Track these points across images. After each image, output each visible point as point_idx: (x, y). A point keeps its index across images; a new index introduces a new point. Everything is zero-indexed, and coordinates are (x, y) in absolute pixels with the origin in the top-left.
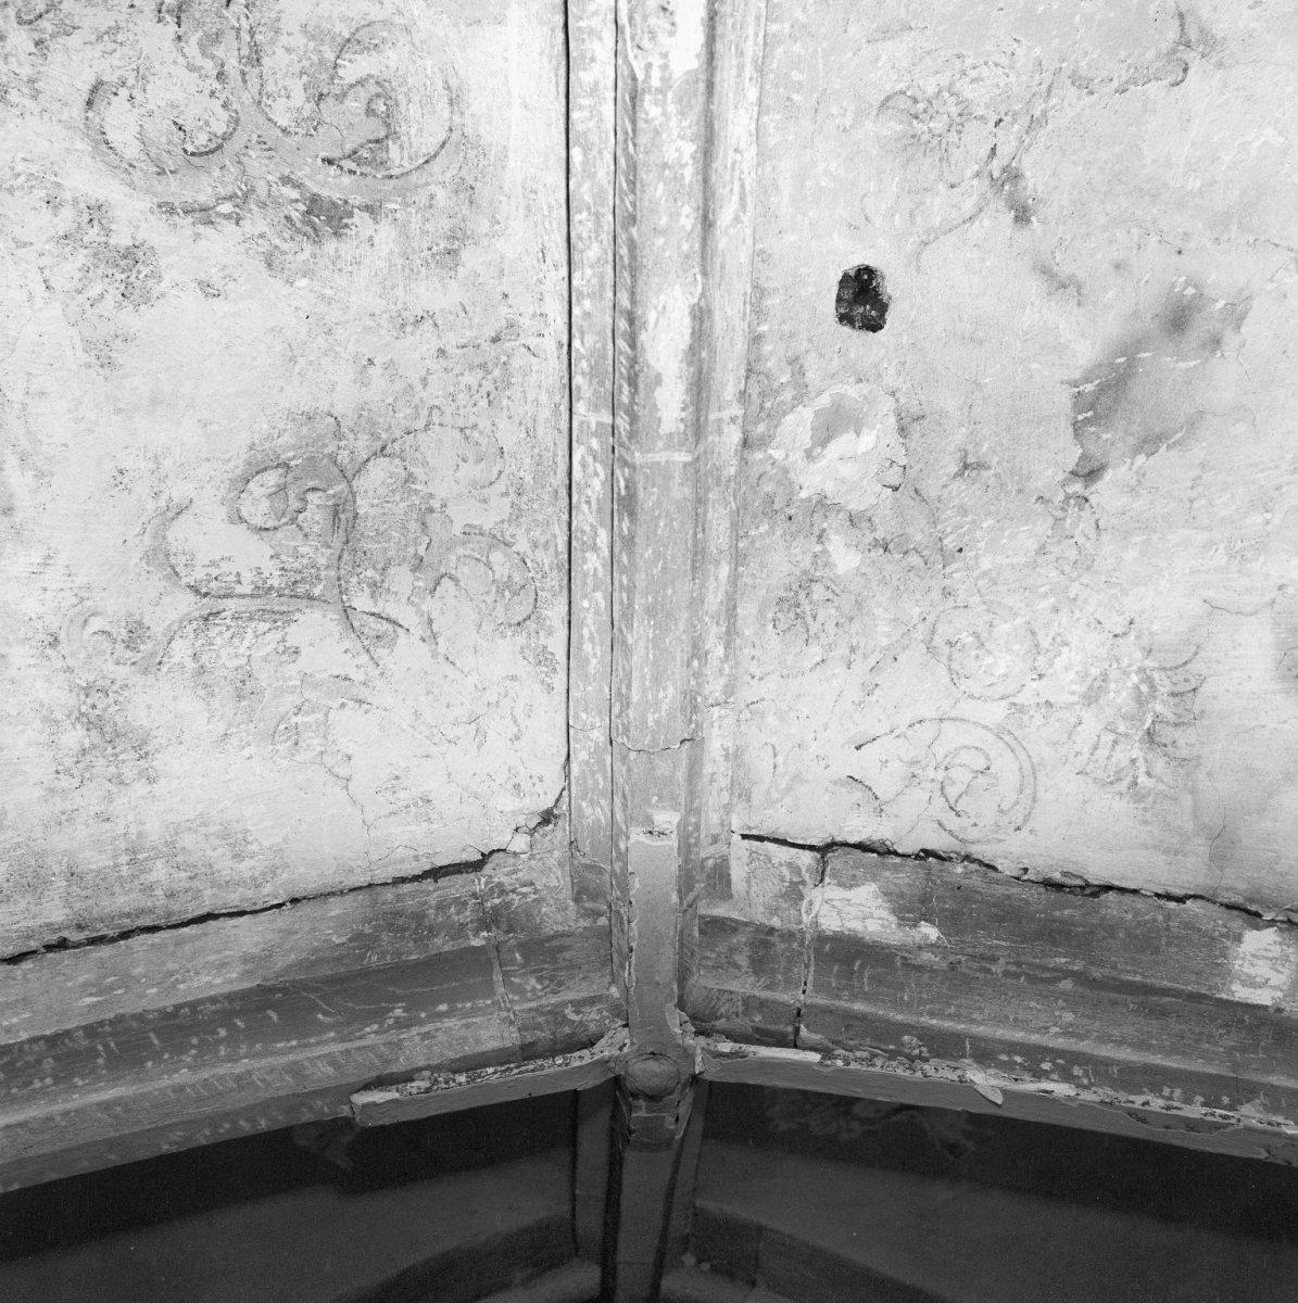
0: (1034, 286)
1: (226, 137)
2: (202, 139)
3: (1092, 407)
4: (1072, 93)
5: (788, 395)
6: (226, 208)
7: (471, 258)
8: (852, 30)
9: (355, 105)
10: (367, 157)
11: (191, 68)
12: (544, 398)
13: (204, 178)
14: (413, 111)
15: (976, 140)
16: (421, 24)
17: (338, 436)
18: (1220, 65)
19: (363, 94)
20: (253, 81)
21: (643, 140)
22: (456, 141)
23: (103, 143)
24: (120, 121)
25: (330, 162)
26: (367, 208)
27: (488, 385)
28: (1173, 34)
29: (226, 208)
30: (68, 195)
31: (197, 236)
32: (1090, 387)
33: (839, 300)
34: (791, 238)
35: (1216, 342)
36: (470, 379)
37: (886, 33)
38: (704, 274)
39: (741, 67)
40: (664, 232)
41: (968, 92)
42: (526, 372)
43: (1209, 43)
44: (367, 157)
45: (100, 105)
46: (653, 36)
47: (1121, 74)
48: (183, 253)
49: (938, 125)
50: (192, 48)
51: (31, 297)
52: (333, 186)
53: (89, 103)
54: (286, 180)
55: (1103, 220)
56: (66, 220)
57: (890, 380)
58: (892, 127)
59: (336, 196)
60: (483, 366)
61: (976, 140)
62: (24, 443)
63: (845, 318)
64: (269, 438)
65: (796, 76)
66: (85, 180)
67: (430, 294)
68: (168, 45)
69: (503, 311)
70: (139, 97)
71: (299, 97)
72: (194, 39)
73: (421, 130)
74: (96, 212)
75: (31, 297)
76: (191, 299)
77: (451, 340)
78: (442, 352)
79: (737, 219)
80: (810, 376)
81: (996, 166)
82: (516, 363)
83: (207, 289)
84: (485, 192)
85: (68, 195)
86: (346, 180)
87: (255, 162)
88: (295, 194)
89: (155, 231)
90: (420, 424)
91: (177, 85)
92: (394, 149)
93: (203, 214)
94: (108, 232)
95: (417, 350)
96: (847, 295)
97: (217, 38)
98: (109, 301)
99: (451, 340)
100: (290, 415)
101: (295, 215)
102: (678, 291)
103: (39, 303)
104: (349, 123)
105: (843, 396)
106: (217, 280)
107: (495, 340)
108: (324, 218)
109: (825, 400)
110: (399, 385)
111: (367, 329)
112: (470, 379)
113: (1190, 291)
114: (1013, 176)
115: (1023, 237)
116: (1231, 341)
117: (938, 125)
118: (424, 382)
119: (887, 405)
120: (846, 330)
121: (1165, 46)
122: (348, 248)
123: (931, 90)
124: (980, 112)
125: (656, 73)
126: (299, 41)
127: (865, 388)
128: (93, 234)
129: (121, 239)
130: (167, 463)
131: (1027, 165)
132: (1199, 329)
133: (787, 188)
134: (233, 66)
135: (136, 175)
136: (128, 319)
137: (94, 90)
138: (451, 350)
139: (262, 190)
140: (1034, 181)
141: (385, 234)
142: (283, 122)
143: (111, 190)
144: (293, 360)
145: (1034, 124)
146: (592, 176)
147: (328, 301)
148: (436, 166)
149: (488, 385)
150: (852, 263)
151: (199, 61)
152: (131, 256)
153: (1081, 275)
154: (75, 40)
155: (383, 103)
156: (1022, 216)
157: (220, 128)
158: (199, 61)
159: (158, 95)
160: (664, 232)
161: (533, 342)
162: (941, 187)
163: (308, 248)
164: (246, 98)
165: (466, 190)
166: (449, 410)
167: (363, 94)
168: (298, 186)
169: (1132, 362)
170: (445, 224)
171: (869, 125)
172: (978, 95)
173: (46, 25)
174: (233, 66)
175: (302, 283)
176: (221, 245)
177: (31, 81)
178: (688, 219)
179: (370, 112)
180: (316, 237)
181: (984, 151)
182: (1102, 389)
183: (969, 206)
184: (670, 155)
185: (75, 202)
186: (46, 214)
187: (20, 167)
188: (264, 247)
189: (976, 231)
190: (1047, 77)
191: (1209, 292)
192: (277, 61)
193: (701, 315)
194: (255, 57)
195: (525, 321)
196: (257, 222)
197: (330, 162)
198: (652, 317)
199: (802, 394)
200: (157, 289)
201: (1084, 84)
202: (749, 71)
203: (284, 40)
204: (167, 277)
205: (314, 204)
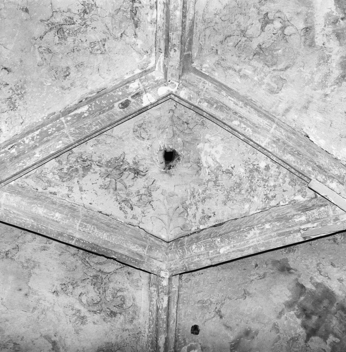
0: (223, 327)
1: (99, 302)
2: (96, 302)
3: (233, 347)
4: (228, 300)
5: (183, 344)
6: (98, 312)
7: (135, 322)
8: (193, 292)
9: (119, 299)
10: (121, 306)
11: (95, 292)
12: (145, 343)
13: (96, 307)
14: (128, 300)
15: (213, 307)
16: (130, 289)
17: (112, 346)
18: (251, 297)
19: (120, 297)
20: (104, 294)
21: (159, 315)
22: (134, 305)
23: (81, 301)
24: (84, 299)
25: (114, 306)
26: (119, 313)
27: (136, 340)
28: (243, 292)
29: (98, 312)
30: (75, 308)
31: (94, 315)
32: (233, 344)
33: (191, 330)
34: (184, 321)
35: (253, 338)
36: (134, 339)
37: (199, 292)
38: (167, 333)
39: (174, 303)
40: (161, 327)
41: (212, 300)
42: (142, 339)
43: (249, 294)
44: (121, 306)
45: (81, 296)
46: (161, 302)
47: (236, 298)
48: (91, 318)
49: (207, 304)
50: (96, 289)
51: (67, 323)
52: (115, 309)
53: (80, 296)
54: (108, 308)
55: (234, 318)
56: (74, 312)
57: (200, 342)
58: (200, 305)
59: (115, 311)
60: (136, 337)
61: (213, 307)
62: (63, 345)
63: (192, 333)
64: (101, 346)
65: (184, 299)
66: (78, 306)
67: (128, 326)
68: (92, 289)
69: (139, 330)
70: (87, 295)
71: (111, 297)
72: (96, 288)
73: (128, 303)
74: (79, 311)
75: (67, 323)
76: (92, 325)
77: (131, 333)
78: (129, 335)
79: (173, 323)
80: (187, 341)
81: (217, 310)
82: (141, 338)
83: (94, 323)
84: (137, 313)
85: (75, 308)
86: (117, 309)
87: (103, 305)
88: (109, 310)
89: (87, 314)
90: (125, 345)
91: (93, 294)
92: (124, 306)
93: (95, 312)
94: (80, 314)
95: (126, 334)
96: (193, 329)
97: (100, 288)
98: (79, 324)
99: (131, 333)
100: (105, 343)
101: (109, 313)
102: (163, 335)
103: (68, 324)
104: (118, 301)
105: (192, 344)
106: (96, 321)
107: (138, 334)
108: (113, 314)
109: (189, 345)
110: (122, 339)
111: (118, 331)
112: (134, 339)
113: (249, 329)
114: (219, 311)
115: (221, 320)
116: (256, 337)
117: (207, 304)
118: (126, 339)
119: (199, 346)
120: (192, 334)
121: (242, 294)
122: (116, 319)
123: (206, 299)
124: (214, 302)
125: (161, 307)
126: (112, 290)
127: (196, 343)
128: (78, 314)
129: (82, 315)
130: (85, 349)
131: (222, 310)
132: (251, 335)
133: (183, 314)
134: (101, 292)
135: (86, 306)
136: (82, 327)
137: (81, 294)
138: (131, 335)
139: (104, 309)
140: (223, 312)
141: (122, 317)
142: (108, 300)
143: (82, 308)
144: (106, 334)
145: (223, 304)
146: (152, 316)
147: (112, 326)
148: (130, 308)
149: (136, 340)
150: (194, 324)
151: (97, 291)
152: (83, 318)
153: (231, 326)
154: (79, 287)
155: (123, 299)
156: (221, 317)
157: (99, 300)
158: (97, 291)
159: (90, 295)
160: (161, 327)
161: (143, 335)
162: (208, 313)
163: (110, 318)
164: (103, 297)
165: (135, 312)
166: (130, 344)
167: (120, 297)
168: (109, 309)
169: (240, 340)
170: (131, 316)
171: (196, 305)
172: (213, 300)
173: (75, 285)
174: (101, 292)
175: (109, 323)
176: (97, 317)
177: (72, 292)
178: (165, 326)
179: (121, 300)
180: (112, 317)
181: (215, 308)
182: (235, 344)
183: (212, 316)
184: (163, 317)
185: (76, 309)
186: (71, 311)
187: (68, 304)
188: (104, 317)
189: (214, 319)
190: (224, 298)
191: (252, 330)
192: (108, 292)
193: (167, 339)
194: (105, 291)
195: (142, 332)
196: (103, 314)
197: (114, 306)
198: (159, 339)
199: (185, 344)
200: (87, 323)
201: (230, 299)
202: (175, 303)
203: (109, 289)
204: (88, 321)
205: (112, 312)
